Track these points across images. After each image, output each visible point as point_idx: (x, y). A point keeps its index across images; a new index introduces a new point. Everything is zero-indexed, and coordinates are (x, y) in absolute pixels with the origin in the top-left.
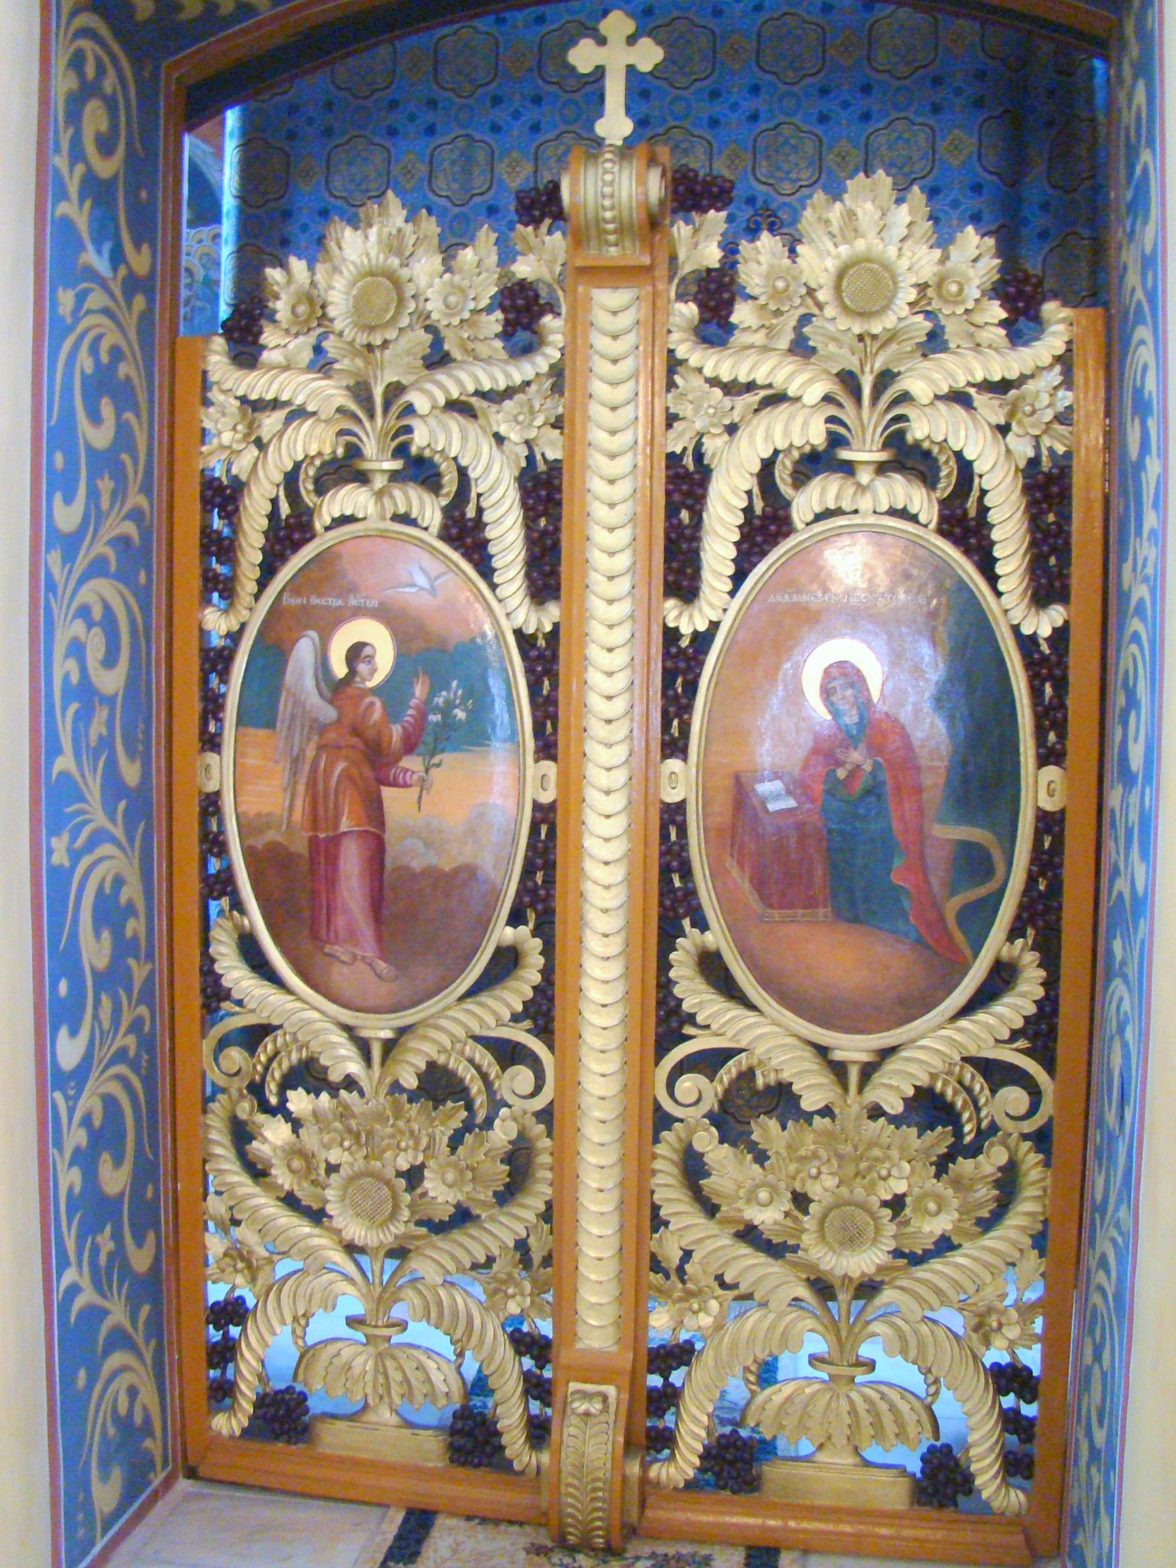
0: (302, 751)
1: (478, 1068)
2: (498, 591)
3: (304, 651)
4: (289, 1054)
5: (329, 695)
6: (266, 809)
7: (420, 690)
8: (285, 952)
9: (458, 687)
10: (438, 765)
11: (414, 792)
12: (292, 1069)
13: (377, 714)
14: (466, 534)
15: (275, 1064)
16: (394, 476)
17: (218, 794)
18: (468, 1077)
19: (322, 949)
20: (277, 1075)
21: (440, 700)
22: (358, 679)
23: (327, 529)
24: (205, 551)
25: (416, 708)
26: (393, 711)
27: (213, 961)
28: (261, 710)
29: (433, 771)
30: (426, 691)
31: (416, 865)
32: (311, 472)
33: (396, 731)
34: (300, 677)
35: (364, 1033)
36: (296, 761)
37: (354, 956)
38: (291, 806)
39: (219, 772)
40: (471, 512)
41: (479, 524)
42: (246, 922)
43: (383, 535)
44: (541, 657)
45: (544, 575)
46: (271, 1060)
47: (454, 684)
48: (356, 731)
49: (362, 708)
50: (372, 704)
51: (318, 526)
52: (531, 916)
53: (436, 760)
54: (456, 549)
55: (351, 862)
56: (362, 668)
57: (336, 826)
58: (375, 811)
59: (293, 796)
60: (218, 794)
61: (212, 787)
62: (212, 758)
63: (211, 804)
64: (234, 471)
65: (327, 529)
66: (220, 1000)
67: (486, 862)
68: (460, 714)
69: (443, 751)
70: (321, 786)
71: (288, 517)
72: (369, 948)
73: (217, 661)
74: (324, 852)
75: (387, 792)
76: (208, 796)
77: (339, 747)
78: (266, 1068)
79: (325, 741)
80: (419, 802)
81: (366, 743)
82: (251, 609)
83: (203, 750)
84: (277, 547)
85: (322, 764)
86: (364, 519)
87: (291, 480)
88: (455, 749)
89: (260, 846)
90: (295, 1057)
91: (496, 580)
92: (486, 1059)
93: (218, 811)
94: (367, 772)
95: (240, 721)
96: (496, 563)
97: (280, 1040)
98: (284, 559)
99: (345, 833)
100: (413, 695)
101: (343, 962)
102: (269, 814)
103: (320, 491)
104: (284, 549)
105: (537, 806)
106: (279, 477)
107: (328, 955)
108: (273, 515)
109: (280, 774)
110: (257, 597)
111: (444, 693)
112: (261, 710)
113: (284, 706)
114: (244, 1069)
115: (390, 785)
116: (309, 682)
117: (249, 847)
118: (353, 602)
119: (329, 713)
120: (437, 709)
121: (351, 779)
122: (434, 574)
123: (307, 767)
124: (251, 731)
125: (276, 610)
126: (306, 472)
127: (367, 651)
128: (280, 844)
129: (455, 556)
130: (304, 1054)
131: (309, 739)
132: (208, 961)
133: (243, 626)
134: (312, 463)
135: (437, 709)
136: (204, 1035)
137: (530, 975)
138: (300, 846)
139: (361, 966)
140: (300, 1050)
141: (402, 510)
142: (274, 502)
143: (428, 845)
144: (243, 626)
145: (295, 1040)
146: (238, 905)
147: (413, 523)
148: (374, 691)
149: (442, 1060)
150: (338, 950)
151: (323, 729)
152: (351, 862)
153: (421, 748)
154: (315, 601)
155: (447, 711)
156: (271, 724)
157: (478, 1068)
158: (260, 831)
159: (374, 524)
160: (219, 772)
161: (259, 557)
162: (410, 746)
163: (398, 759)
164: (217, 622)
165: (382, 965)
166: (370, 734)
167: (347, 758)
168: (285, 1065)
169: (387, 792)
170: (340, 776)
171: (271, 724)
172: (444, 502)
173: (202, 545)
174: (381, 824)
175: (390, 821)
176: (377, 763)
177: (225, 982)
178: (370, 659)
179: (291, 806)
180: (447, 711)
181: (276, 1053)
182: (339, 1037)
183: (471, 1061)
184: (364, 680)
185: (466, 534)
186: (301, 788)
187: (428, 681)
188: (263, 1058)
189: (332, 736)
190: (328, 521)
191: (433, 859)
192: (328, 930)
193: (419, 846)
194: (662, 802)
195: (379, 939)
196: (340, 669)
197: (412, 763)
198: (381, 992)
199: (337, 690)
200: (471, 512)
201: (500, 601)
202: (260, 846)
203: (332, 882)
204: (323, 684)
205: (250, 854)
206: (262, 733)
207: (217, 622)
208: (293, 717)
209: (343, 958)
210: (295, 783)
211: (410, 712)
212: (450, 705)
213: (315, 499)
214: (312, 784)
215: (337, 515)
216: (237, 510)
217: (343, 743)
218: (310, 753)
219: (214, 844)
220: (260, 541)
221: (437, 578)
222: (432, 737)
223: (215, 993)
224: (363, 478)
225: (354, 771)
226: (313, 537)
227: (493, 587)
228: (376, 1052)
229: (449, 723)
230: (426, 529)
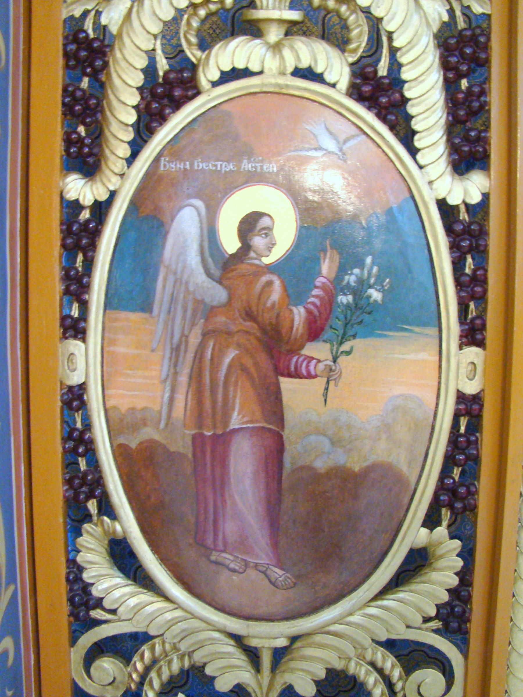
0: (184, 337)
1: (380, 671)
2: (419, 157)
3: (186, 223)
4: (170, 662)
5: (217, 273)
6: (140, 404)
7: (327, 268)
8: (165, 560)
9: (373, 263)
10: (348, 353)
11: (319, 383)
12: (172, 679)
13: (276, 294)
14: (379, 92)
15: (153, 674)
16: (292, 29)
17: (82, 387)
18: (363, 672)
19: (208, 557)
20: (156, 684)
21: (351, 279)
22: (252, 254)
23: (215, 84)
24: (68, 109)
25: (323, 288)
26: (294, 294)
27: (81, 569)
28: (133, 293)
29: (342, 360)
30: (335, 269)
31: (321, 465)
32: (195, 24)
33: (299, 314)
34: (182, 252)
35: (254, 643)
36: (177, 351)
37: (246, 564)
38: (171, 400)
39: (83, 362)
40: (383, 69)
41: (396, 82)
42: (118, 527)
43: (279, 93)
44: (467, 231)
45: (466, 139)
46: (148, 669)
47: (369, 260)
48: (249, 315)
49: (258, 287)
50: (270, 283)
51: (203, 82)
52: (446, 514)
53: (345, 347)
54: (369, 108)
55: (244, 462)
56: (258, 242)
57: (226, 418)
58: (273, 405)
59: (173, 391)
60: (82, 387)
61: (75, 379)
62: (75, 346)
63: (75, 398)
64: (104, 21)
65: (215, 84)
66: (89, 608)
67: (402, 461)
68: (376, 295)
69: (354, 336)
70: (207, 380)
71: (166, 73)
72: (263, 554)
73: (80, 232)
74: (212, 448)
75: (286, 384)
76: (71, 388)
77: (229, 334)
78: (143, 677)
79: (211, 327)
80: (325, 395)
81: (263, 330)
82: (122, 175)
83: (65, 337)
84: (155, 105)
85: (208, 354)
86: (261, 73)
87: (170, 31)
88: (369, 334)
89: (133, 445)
90: (176, 667)
91: (417, 144)
92: (389, 663)
93: (83, 405)
94: (263, 358)
95: (109, 304)
96: (416, 125)
97: (158, 649)
98: (163, 119)
99: (235, 431)
100: (319, 274)
101: (234, 571)
102: (145, 409)
103: (205, 45)
104: (163, 108)
105: (461, 397)
106: (156, 28)
107: (216, 563)
108: (150, 71)
109: (159, 367)
110: (131, 160)
111: (356, 271)
112: (133, 293)
113: (162, 289)
114: (118, 679)
115: (290, 375)
116: (193, 259)
117: (120, 446)
118: (247, 166)
119: (218, 294)
120: (346, 289)
121: (244, 369)
122: (342, 137)
123: (190, 356)
124: (122, 315)
125: (151, 177)
126: (189, 23)
127: (264, 222)
128: (156, 442)
129: (370, 117)
130: (187, 664)
131: (193, 324)
132: (75, 570)
133: (113, 194)
134: (195, 14)
135: (346, 289)
136: (73, 641)
137: (442, 578)
138: (181, 443)
139: (252, 573)
140: (181, 658)
141: (304, 64)
142: (151, 54)
143: (335, 442)
144: (113, 194)
145: (175, 648)
146: (107, 508)
147: (319, 78)
148: (270, 269)
149: (339, 665)
150: (226, 557)
151: (211, 312)
152: (244, 462)
153: (328, 333)
154: (200, 165)
155: (359, 291)
156: (146, 307)
157: (380, 671)
158: (135, 427)
159: (269, 81)
160: (83, 362)
161: (132, 118)
162: (314, 332)
163: (302, 347)
164: (80, 189)
165: (277, 573)
166: (267, 317)
167: (239, 345)
168: (165, 676)
169: (286, 384)
170: (230, 366)
171: (146, 307)
172: (351, 59)
173: (64, 104)
174: (280, 420)
175: (288, 416)
176: (277, 352)
177: (96, 591)
178: (268, 231)
179: (171, 400)
180: (359, 291)
181: (155, 661)
182: (229, 647)
183: (372, 664)
184: (260, 256)
185: (379, 92)
186: (183, 379)
187: (337, 257)
188: (139, 666)
189: (221, 319)
190: (215, 76)
191: (340, 458)
192: (216, 536)
193: (326, 445)
194: (484, 349)
195: (275, 544)
196: (231, 244)
197: (318, 351)
198: (276, 600)
199: (227, 267)
200: (383, 69)
201: (421, 167)
202: (133, 445)
203: (221, 483)
204: (210, 260)
205: (122, 454)
206: (134, 316)
207: (80, 189)
208: (173, 300)
209: (232, 566)
210: (176, 374)
211: (316, 292)
212: (363, 284)
213: (199, 53)
214: (197, 376)
215: (227, 68)
216: (106, 65)
217: (233, 328)
218: (195, 339)
219: (79, 442)
220: (134, 99)
221: (345, 142)
222: (341, 319)
223: (83, 604)
224: (254, 30)
225: (248, 362)
226: (198, 93)
227: (413, 152)
228: (266, 660)
229: (361, 306)
230: (333, 86)
